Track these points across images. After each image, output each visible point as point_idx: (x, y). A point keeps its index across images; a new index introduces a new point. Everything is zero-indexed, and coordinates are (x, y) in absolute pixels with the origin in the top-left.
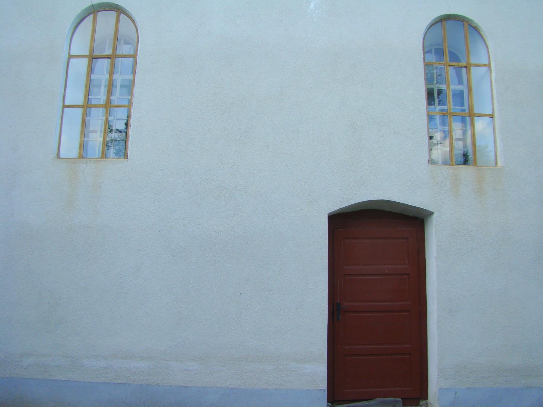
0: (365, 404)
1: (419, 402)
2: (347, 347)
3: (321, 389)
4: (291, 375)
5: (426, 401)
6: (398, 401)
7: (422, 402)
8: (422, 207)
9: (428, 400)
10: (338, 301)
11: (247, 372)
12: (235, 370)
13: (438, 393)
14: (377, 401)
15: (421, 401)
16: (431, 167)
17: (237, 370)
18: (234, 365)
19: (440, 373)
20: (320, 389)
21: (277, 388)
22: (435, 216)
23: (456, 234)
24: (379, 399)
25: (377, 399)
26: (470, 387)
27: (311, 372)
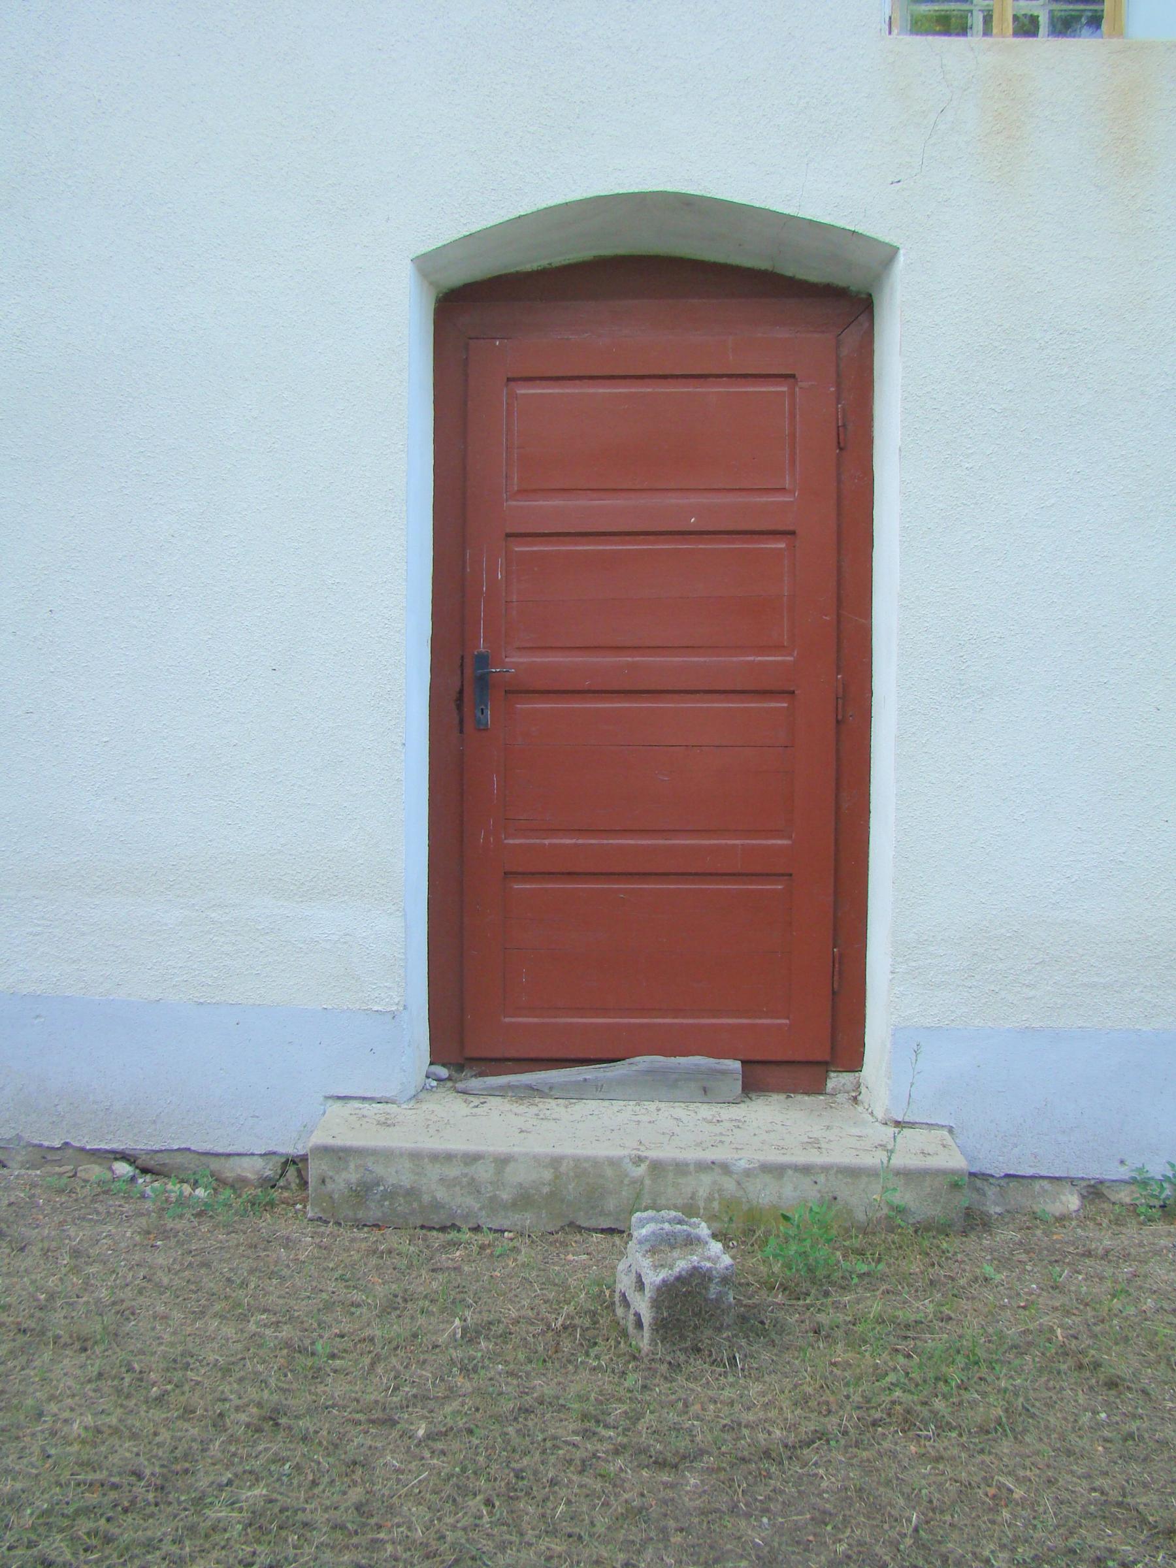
0: (580, 1078)
1: (825, 1079)
2: (517, 841)
3: (380, 1008)
4: (258, 949)
5: (857, 1074)
6: (724, 1072)
7: (837, 1080)
8: (841, 224)
9: (862, 1074)
10: (482, 647)
11: (83, 934)
12: (39, 925)
13: (888, 1045)
14: (634, 1068)
15: (832, 1075)
16: (1105, 26)
17: (49, 923)
18: (36, 901)
19: (900, 960)
20: (376, 1008)
21: (202, 1001)
22: (901, 260)
23: (997, 344)
24: (643, 1062)
25: (638, 1059)
26: (1036, 1025)
27: (335, 938)
